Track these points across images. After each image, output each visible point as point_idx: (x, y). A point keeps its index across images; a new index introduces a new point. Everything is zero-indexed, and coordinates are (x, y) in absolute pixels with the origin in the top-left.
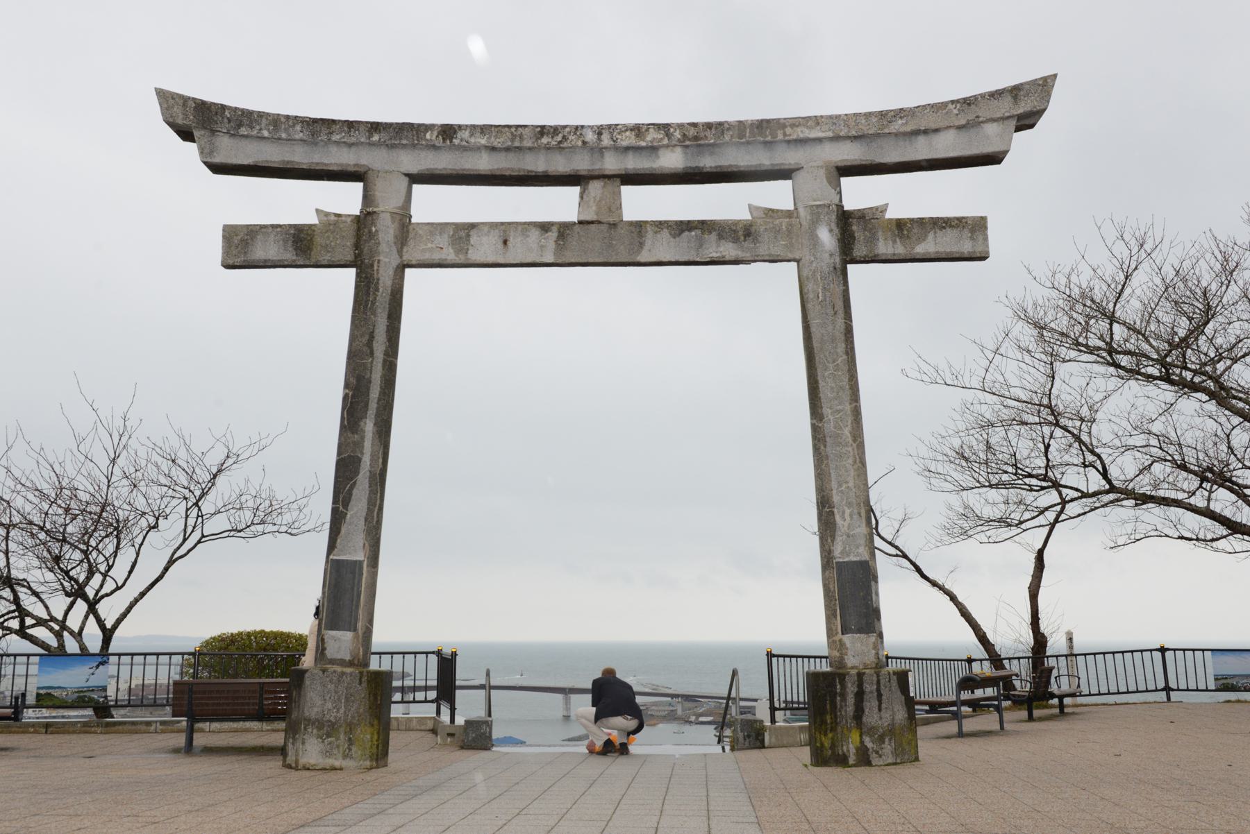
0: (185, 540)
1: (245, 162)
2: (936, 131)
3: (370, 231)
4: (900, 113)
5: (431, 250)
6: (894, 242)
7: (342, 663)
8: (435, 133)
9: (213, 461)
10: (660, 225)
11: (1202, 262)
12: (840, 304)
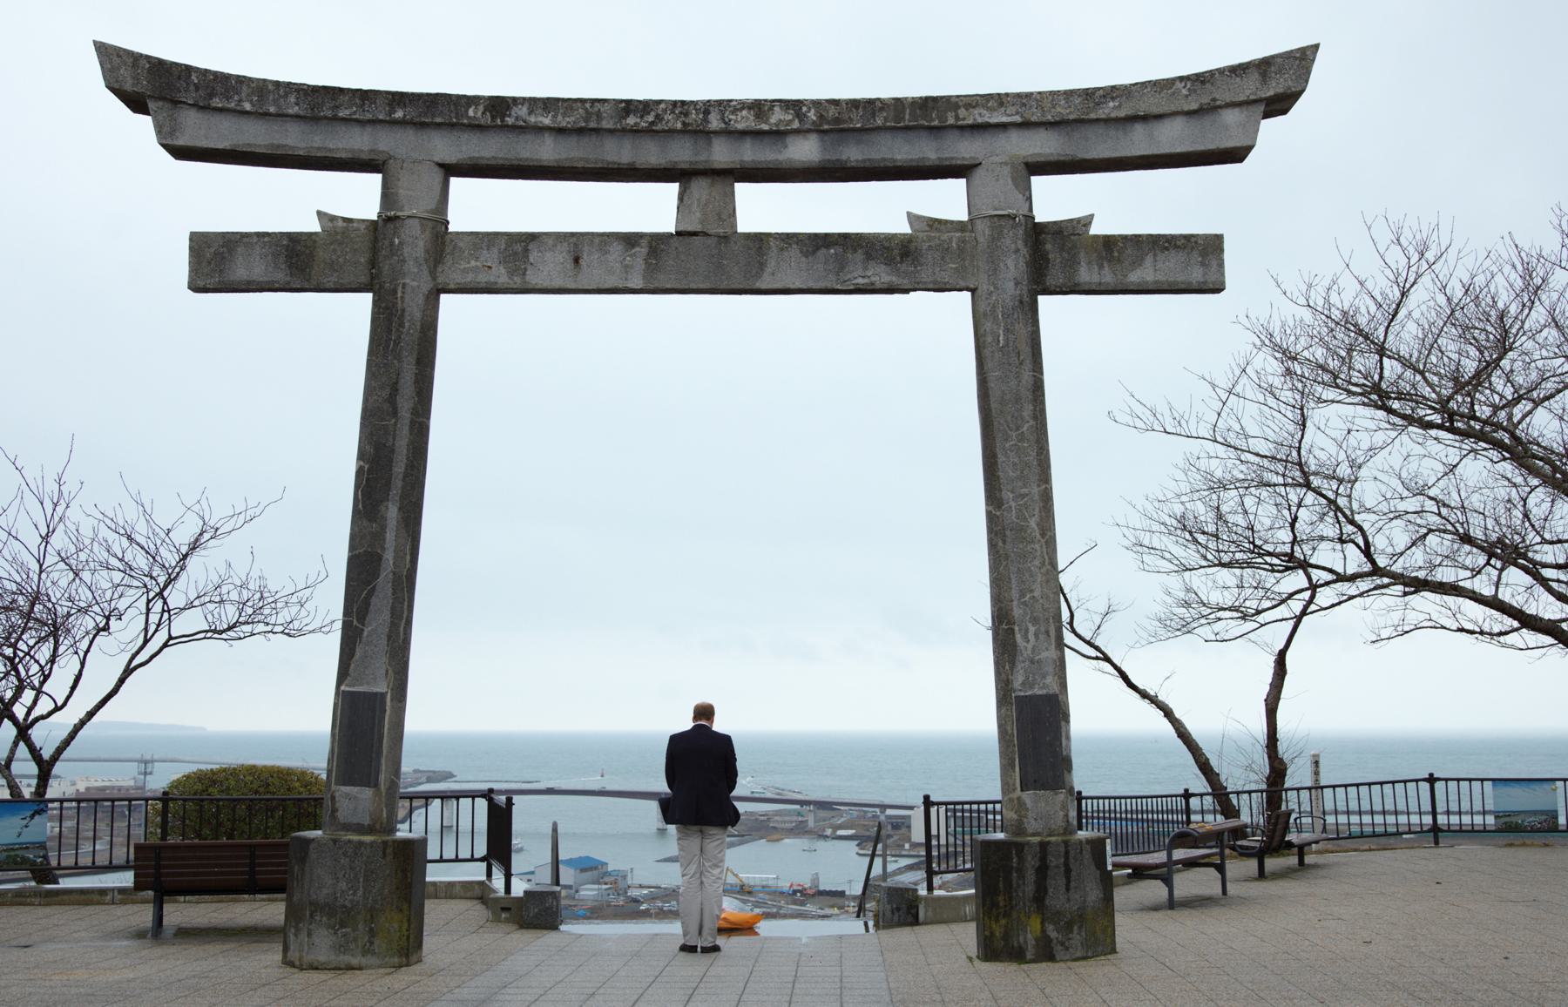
0: (146, 641)
1: (220, 146)
2: (1159, 117)
3: (392, 244)
4: (1113, 92)
5: (475, 270)
6: (1101, 267)
7: (360, 829)
8: (481, 108)
9: (183, 537)
10: (788, 239)
11: (1499, 279)
12: (1026, 350)
